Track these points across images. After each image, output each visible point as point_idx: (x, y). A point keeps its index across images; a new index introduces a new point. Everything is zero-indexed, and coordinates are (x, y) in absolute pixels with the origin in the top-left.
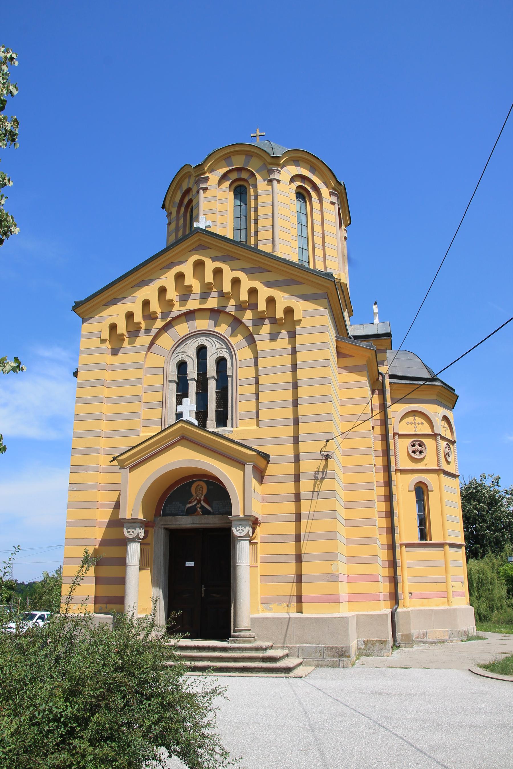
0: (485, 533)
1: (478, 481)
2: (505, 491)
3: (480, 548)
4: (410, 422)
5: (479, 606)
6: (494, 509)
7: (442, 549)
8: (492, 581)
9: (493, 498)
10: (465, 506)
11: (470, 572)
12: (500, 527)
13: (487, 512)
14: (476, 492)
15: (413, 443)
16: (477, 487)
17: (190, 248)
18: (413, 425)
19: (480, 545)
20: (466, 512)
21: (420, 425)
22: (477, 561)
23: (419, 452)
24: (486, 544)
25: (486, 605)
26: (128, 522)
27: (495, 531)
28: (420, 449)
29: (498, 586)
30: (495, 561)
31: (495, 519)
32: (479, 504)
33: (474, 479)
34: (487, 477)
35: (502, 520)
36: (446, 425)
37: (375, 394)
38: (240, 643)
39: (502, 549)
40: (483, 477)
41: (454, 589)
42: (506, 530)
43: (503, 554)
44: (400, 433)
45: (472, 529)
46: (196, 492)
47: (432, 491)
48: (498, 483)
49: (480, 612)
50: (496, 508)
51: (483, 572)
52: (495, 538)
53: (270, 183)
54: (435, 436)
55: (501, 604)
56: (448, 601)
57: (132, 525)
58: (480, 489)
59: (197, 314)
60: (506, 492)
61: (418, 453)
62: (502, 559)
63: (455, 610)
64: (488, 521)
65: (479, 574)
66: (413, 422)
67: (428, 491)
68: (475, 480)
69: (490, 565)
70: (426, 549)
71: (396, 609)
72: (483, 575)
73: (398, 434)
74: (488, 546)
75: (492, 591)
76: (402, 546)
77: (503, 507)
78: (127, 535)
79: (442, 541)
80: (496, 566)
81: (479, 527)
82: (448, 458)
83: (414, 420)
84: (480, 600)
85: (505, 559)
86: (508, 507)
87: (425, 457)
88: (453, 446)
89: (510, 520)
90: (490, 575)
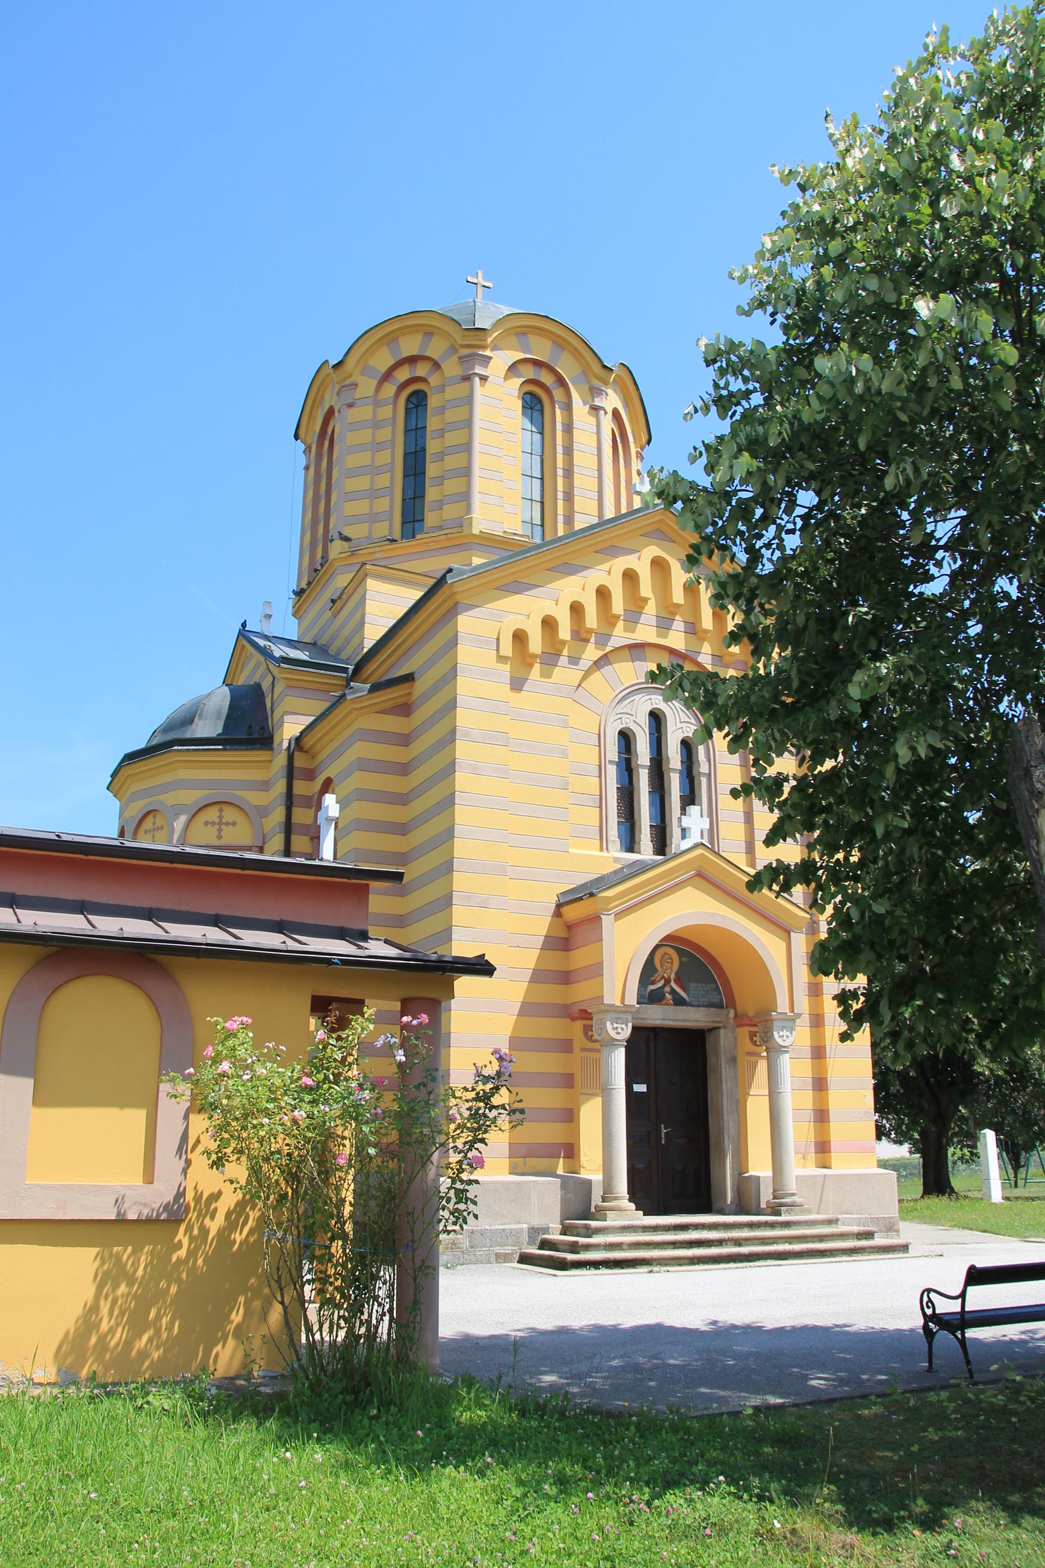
17: (644, 531)
26: (615, 1011)
38: (796, 1215)
46: (662, 966)
53: (594, 412)
57: (621, 1015)
59: (648, 651)
78: (613, 1034)
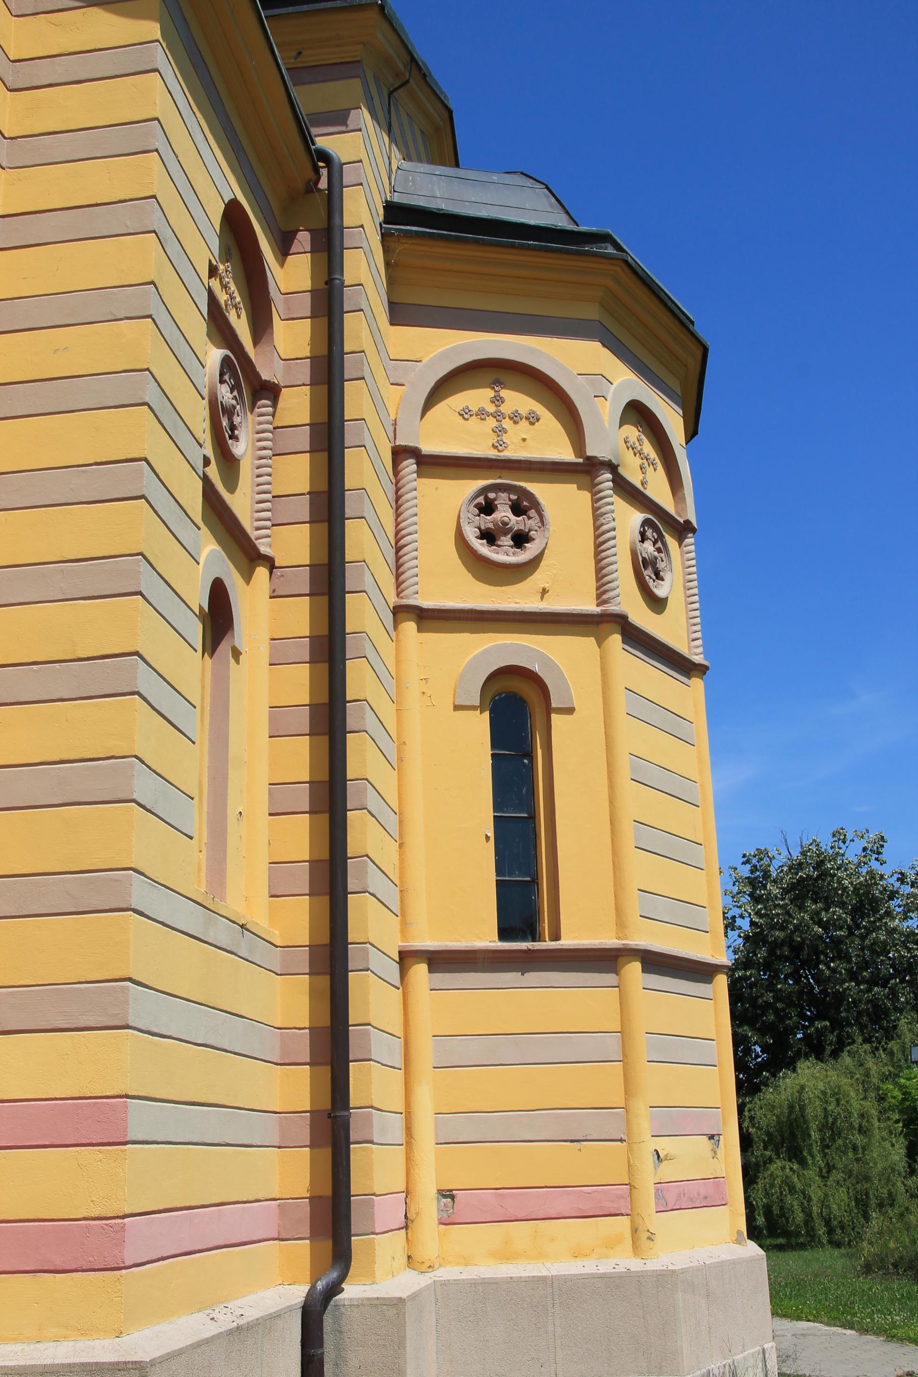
0: (845, 990)
1: (826, 843)
2: (896, 876)
3: (830, 1029)
4: (474, 409)
5: (826, 1195)
6: (869, 922)
7: (609, 978)
8: (864, 1123)
9: (867, 893)
10: (790, 916)
11: (800, 1099)
12: (884, 972)
13: (851, 934)
14: (819, 877)
15: (486, 498)
16: (822, 862)
18: (492, 423)
19: (830, 1022)
20: (791, 930)
21: (524, 424)
22: (820, 1065)
23: (513, 539)
24: (847, 1018)
25: (848, 1193)
27: (873, 982)
28: (516, 522)
29: (882, 1138)
30: (870, 1063)
31: (873, 952)
32: (827, 910)
33: (814, 841)
34: (849, 837)
35: (891, 955)
36: (648, 449)
37: (293, 250)
39: (890, 1033)
40: (839, 836)
41: (668, 1172)
42: (903, 981)
43: (893, 1045)
44: (428, 447)
45: (808, 980)
47: (570, 711)
48: (879, 853)
49: (831, 1213)
50: (874, 922)
51: (837, 1095)
52: (873, 1002)
54: (588, 473)
55: (889, 1191)
56: (635, 1231)
58: (831, 869)
60: (902, 879)
61: (506, 541)
62: (892, 1060)
63: (664, 1278)
64: (851, 957)
65: (826, 1102)
66: (491, 409)
67: (548, 710)
68: (818, 845)
69: (858, 1076)
70: (533, 977)
71: (334, 1289)
72: (838, 1104)
73: (413, 452)
74: (851, 1025)
75: (863, 1153)
76: (408, 961)
77: (893, 918)
79: (609, 941)
80: (875, 1080)
81: (827, 973)
82: (651, 584)
83: (498, 400)
84: (828, 1177)
85: (900, 1060)
86: (906, 918)
87: (542, 554)
88: (680, 545)
89: (911, 953)
90: (858, 1106)
